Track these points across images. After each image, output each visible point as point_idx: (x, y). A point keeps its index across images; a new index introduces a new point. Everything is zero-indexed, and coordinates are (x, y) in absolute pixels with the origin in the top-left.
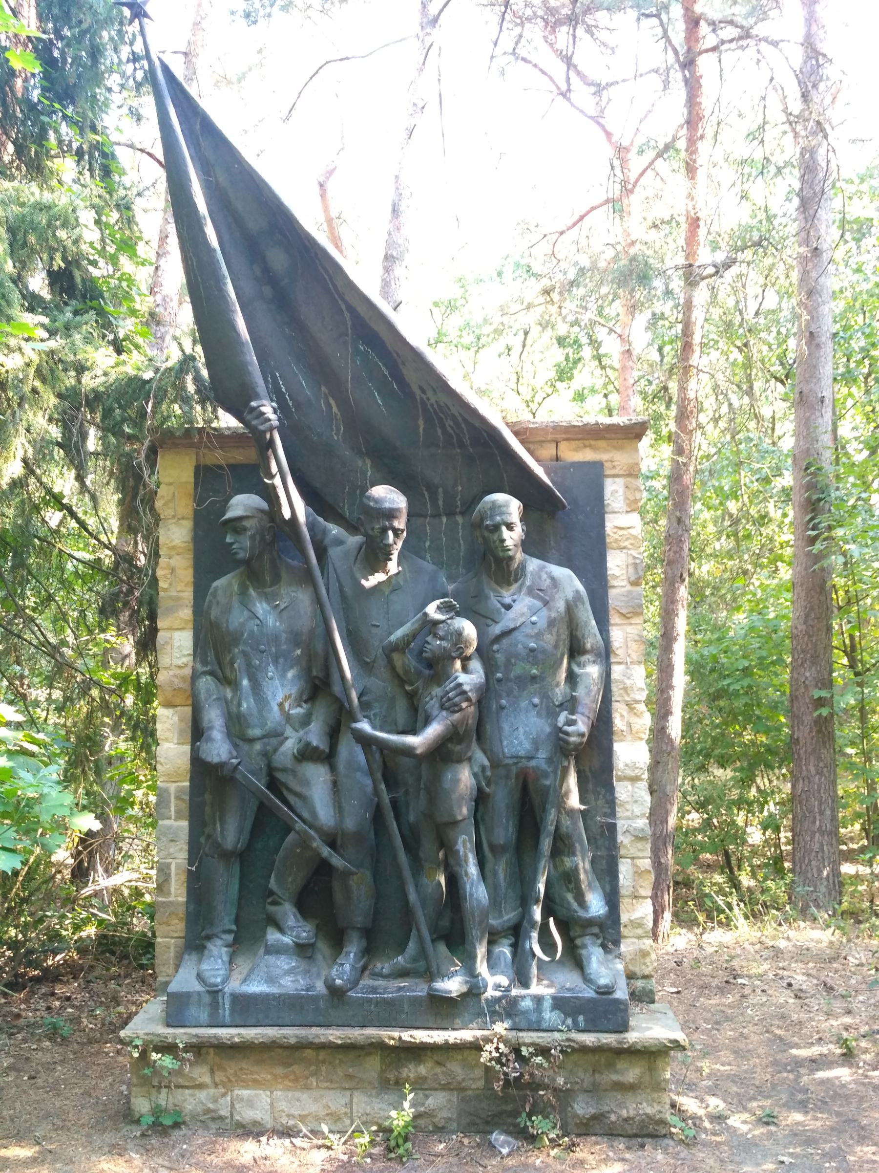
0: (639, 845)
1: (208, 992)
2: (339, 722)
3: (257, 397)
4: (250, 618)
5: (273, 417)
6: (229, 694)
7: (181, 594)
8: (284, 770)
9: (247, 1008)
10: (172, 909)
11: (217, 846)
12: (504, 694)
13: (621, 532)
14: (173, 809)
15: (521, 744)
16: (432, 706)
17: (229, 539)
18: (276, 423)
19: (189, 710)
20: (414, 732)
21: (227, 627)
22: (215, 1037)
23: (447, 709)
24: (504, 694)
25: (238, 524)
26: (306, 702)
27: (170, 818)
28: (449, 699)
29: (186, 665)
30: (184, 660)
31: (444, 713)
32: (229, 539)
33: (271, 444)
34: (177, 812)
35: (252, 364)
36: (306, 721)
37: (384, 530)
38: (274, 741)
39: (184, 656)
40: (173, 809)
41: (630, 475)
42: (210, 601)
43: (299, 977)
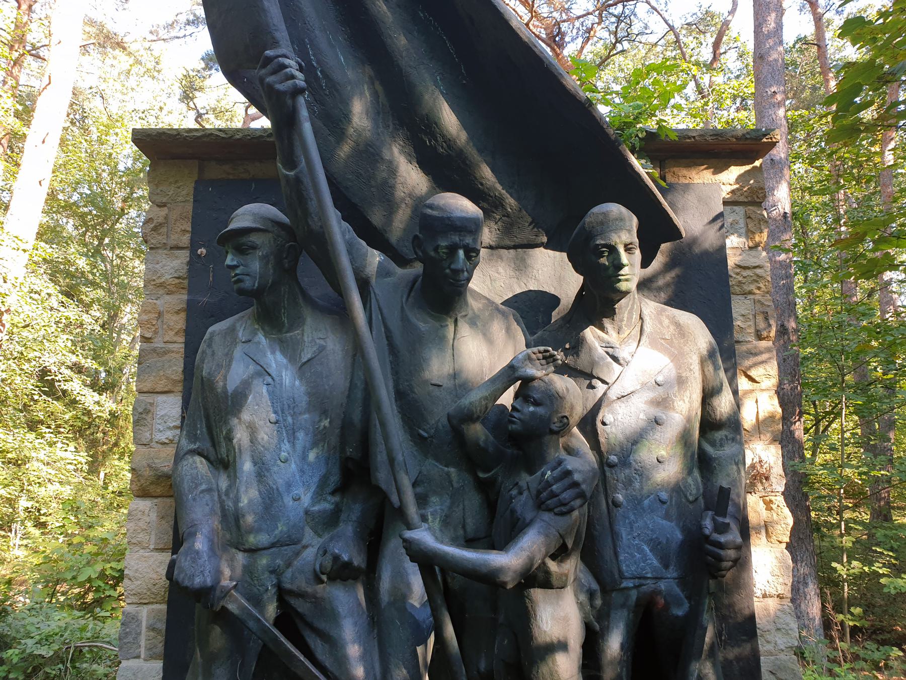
2: (380, 523)
3: (275, 44)
4: (258, 374)
6: (224, 483)
7: (171, 346)
12: (620, 485)
13: (745, 273)
14: (143, 643)
15: (645, 558)
16: (522, 503)
17: (230, 260)
20: (501, 544)
23: (549, 510)
24: (620, 485)
25: (244, 240)
26: (333, 493)
27: (138, 657)
28: (553, 495)
29: (171, 441)
30: (170, 434)
31: (547, 516)
32: (230, 260)
34: (149, 649)
35: (359, 640)
36: (330, 521)
38: (288, 551)
39: (170, 428)
40: (143, 643)
42: (203, 352)
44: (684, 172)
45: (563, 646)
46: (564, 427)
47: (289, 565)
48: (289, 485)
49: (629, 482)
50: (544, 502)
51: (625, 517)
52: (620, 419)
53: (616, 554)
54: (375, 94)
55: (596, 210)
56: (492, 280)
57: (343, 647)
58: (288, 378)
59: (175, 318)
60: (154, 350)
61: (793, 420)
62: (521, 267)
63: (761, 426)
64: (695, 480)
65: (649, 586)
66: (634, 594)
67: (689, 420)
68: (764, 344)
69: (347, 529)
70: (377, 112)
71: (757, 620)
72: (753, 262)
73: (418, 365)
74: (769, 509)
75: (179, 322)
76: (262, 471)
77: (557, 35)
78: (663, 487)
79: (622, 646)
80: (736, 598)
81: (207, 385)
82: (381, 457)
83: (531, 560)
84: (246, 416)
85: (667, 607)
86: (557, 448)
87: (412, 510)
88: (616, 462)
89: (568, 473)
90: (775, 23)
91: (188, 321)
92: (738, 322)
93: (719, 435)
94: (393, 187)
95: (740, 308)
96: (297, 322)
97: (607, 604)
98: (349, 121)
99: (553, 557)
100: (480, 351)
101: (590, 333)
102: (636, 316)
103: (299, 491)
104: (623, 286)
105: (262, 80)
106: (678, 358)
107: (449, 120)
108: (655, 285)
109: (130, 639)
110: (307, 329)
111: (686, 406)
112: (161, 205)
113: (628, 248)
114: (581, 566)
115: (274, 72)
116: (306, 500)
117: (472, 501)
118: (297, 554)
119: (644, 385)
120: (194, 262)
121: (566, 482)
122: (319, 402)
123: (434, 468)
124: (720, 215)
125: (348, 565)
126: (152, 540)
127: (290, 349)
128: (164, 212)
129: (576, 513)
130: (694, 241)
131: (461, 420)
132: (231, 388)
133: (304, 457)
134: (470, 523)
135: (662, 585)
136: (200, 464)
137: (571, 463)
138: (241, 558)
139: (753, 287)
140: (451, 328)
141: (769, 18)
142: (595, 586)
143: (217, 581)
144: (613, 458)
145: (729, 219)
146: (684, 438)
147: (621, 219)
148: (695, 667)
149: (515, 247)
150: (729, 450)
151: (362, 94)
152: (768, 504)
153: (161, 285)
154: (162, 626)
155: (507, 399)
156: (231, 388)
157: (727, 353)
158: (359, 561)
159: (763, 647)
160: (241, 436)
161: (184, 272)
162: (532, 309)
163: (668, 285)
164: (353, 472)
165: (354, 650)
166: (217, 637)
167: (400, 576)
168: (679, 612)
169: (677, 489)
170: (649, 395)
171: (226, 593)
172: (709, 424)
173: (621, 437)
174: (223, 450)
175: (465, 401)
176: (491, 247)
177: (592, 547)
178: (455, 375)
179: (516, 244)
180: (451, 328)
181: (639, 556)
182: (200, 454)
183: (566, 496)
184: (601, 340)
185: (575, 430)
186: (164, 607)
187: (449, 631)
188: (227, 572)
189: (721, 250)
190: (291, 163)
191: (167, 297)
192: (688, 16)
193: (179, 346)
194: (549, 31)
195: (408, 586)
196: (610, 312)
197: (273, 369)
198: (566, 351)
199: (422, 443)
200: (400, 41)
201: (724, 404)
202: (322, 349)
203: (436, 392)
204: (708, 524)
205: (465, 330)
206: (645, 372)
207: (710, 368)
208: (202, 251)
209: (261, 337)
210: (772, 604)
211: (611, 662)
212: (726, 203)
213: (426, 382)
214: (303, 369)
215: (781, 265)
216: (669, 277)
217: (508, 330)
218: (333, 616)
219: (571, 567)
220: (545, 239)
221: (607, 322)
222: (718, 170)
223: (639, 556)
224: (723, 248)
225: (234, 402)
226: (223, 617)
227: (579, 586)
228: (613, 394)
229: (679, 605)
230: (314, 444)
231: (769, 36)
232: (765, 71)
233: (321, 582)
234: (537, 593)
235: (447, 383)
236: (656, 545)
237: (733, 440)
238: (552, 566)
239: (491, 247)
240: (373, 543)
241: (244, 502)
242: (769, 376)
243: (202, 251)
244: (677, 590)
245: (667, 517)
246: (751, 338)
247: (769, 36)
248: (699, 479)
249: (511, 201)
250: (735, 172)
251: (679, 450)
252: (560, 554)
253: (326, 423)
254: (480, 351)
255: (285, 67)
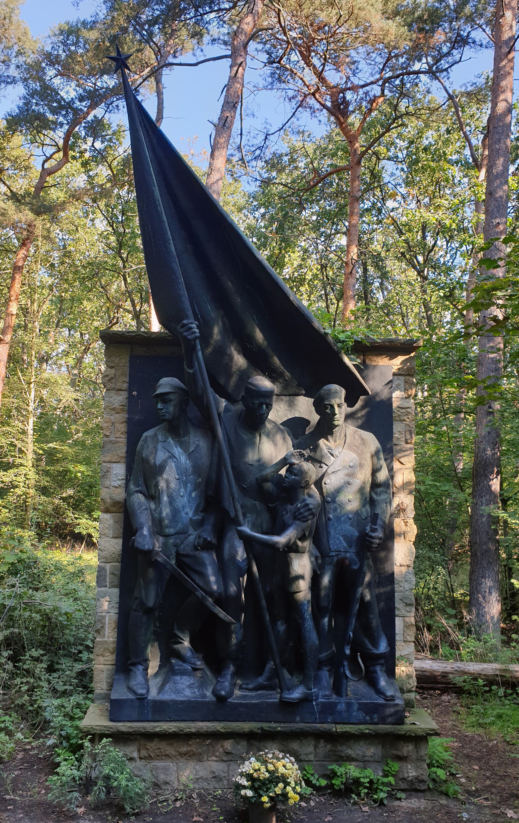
0: (408, 608)
1: (138, 699)
3: (187, 317)
5: (197, 330)
6: (153, 506)
8: (188, 556)
9: (161, 710)
10: (106, 646)
11: (142, 604)
13: (402, 411)
14: (108, 580)
15: (340, 543)
16: (287, 517)
17: (159, 406)
18: (198, 334)
19: (121, 515)
20: (279, 533)
21: (155, 462)
22: (143, 728)
23: (299, 520)
25: (167, 397)
26: (201, 512)
28: (301, 514)
30: (119, 482)
31: (298, 522)
32: (159, 406)
33: (194, 348)
35: (215, 575)
36: (199, 524)
37: (261, 404)
38: (182, 536)
41: (409, 375)
43: (196, 690)
44: (375, 358)
45: (302, 577)
46: (307, 485)
47: (182, 543)
48: (184, 507)
49: (335, 510)
50: (297, 517)
51: (333, 525)
52: (331, 483)
53: (328, 541)
54: (224, 324)
55: (326, 387)
56: (278, 413)
57: (208, 577)
58: (183, 459)
59: (121, 426)
60: (110, 441)
61: (491, 477)
62: (291, 405)
63: (405, 485)
64: (367, 510)
65: (342, 555)
66: (335, 559)
67: (364, 483)
68: (409, 446)
69: (208, 527)
70: (224, 332)
71: (395, 576)
72: (406, 405)
73: (244, 454)
74: (406, 525)
75: (123, 428)
76: (172, 501)
77: (342, 104)
78: (350, 512)
79: (330, 582)
80: (386, 565)
81: (145, 461)
82: (226, 495)
83: (290, 540)
84: (165, 476)
85: (350, 564)
86: (304, 494)
87: (241, 518)
88: (329, 501)
89: (307, 505)
90: (503, 166)
91: (128, 427)
92: (396, 435)
93: (379, 490)
94: (231, 366)
95: (398, 428)
96: (187, 433)
97: (323, 562)
98: (212, 337)
99: (300, 539)
100: (272, 450)
101: (322, 442)
102: (343, 435)
103: (187, 510)
104: (336, 423)
105: (181, 333)
106: (360, 455)
107: (259, 336)
108: (357, 416)
109: (102, 578)
110: (191, 436)
111: (364, 476)
112: (111, 367)
113: (339, 406)
114: (312, 546)
115: (187, 331)
116: (191, 514)
117: (266, 517)
118: (186, 538)
119: (344, 467)
120: (130, 397)
121: (306, 508)
122: (197, 469)
123: (249, 502)
124: (391, 381)
125: (210, 542)
126: (110, 533)
127: (184, 446)
128: (113, 371)
129: (310, 522)
130: (377, 394)
131: (261, 481)
132: (158, 463)
133: (190, 495)
134: (265, 526)
135: (348, 555)
136: (141, 497)
137: (309, 501)
138: (161, 539)
139: (405, 418)
140: (258, 438)
141: (498, 162)
142: (318, 554)
143: (154, 548)
144: (329, 499)
145: (396, 383)
146: (361, 490)
147: (336, 392)
148: (360, 590)
149: (289, 395)
150: (383, 497)
151: (218, 324)
152: (406, 523)
153: (114, 409)
154: (118, 573)
155: (283, 472)
156: (158, 463)
157: (388, 449)
158: (214, 541)
159: (397, 588)
160: (162, 485)
161: (125, 402)
162: (295, 427)
163: (363, 416)
164: (212, 502)
165: (212, 579)
166: (151, 573)
167: (233, 549)
168: (356, 567)
169: (357, 513)
170: (346, 471)
171: (157, 553)
172: (375, 485)
173: (332, 490)
174: (153, 491)
175: (264, 473)
176: (277, 395)
177: (318, 537)
178: (259, 460)
179: (289, 394)
180: (258, 438)
181: (338, 542)
182: (141, 493)
183: (306, 514)
184: (326, 445)
185: (313, 486)
186: (118, 565)
187: (255, 569)
188: (157, 544)
189: (389, 402)
190: (191, 367)
191: (117, 415)
192: (468, 85)
193: (123, 439)
194: (335, 98)
195: (237, 552)
196: (332, 434)
197: (177, 455)
198: (311, 450)
199: (243, 490)
200: (238, 300)
201: (383, 475)
202: (198, 446)
203: (251, 468)
204: (368, 528)
205: (264, 439)
206: (346, 461)
207: (375, 459)
208: (135, 393)
209: (170, 440)
210: (404, 569)
211: (325, 588)
212: (394, 374)
213: (246, 463)
214: (190, 455)
215: (493, 361)
216: (363, 412)
217: (284, 439)
218: (204, 565)
219: (307, 544)
220: (304, 392)
221: (329, 437)
222: (392, 358)
223: (338, 542)
224: (391, 398)
225: (160, 469)
226: (155, 565)
227: (311, 555)
228: (329, 471)
229: (356, 564)
230: (195, 490)
231: (497, 177)
232: (492, 205)
233: (198, 550)
234: (292, 555)
235: (256, 464)
236: (345, 537)
237: (386, 492)
238: (299, 543)
239: (277, 395)
240: (220, 534)
241: (164, 514)
242: (410, 462)
243: (135, 393)
244: (355, 557)
245: (352, 525)
246: (403, 443)
247: (497, 177)
248: (369, 510)
249: (287, 374)
250: (400, 359)
251: (358, 496)
252: (302, 538)
253: (200, 480)
254: (272, 450)
255: (192, 328)
